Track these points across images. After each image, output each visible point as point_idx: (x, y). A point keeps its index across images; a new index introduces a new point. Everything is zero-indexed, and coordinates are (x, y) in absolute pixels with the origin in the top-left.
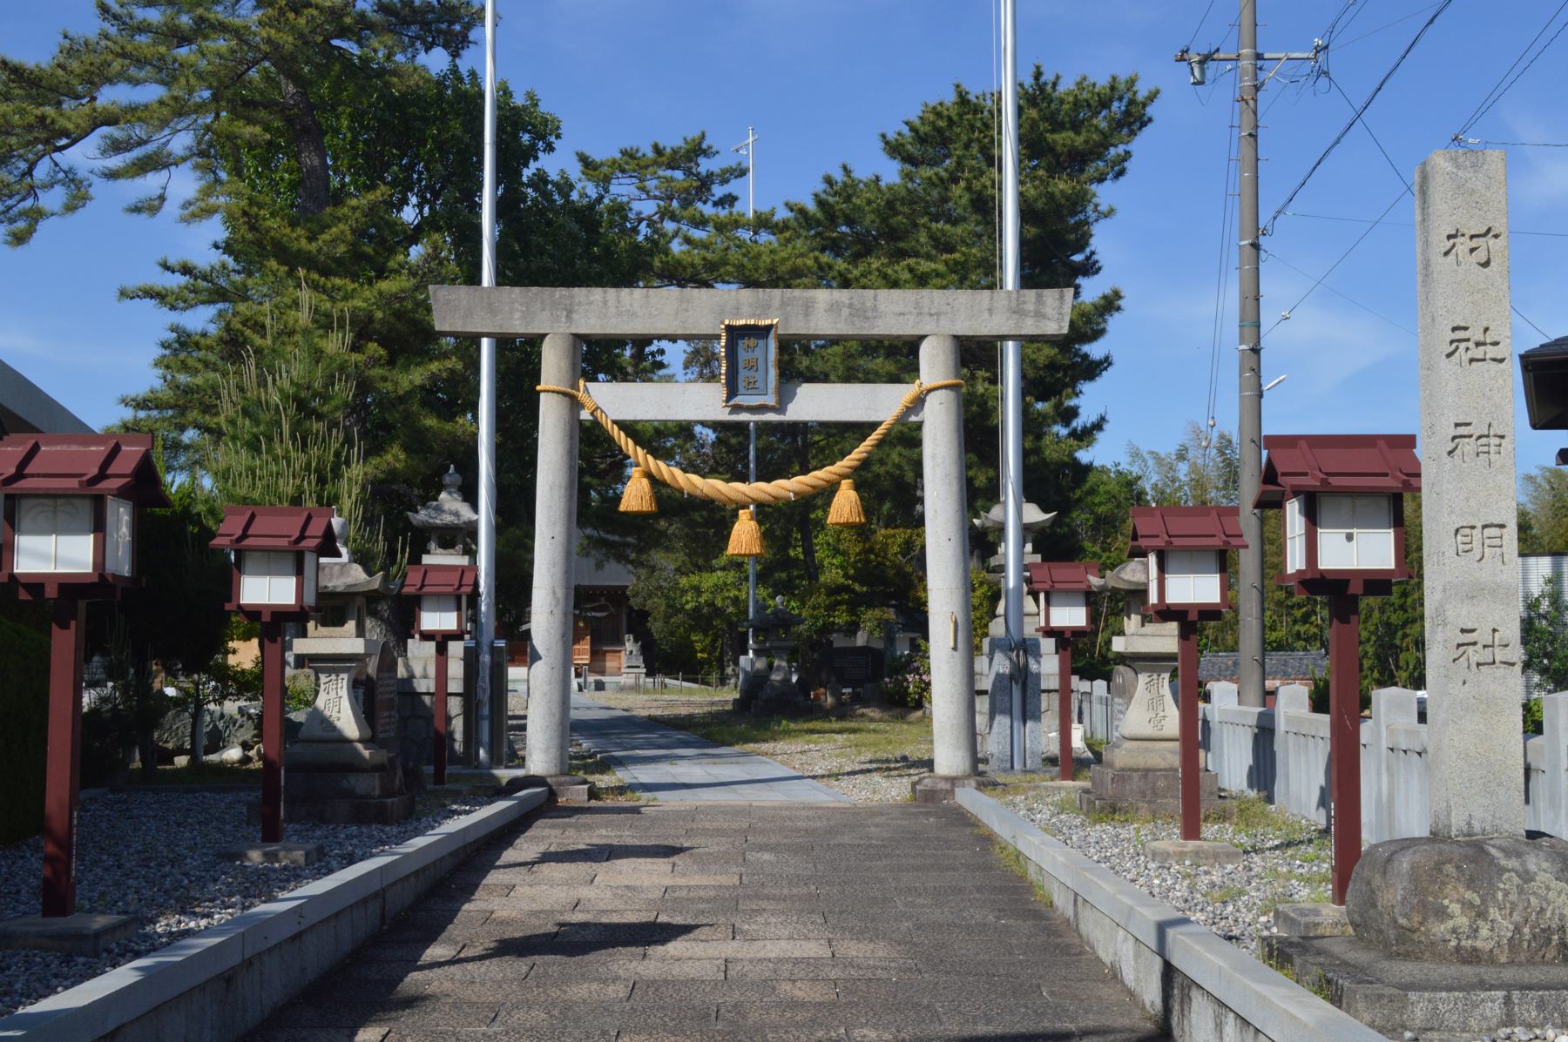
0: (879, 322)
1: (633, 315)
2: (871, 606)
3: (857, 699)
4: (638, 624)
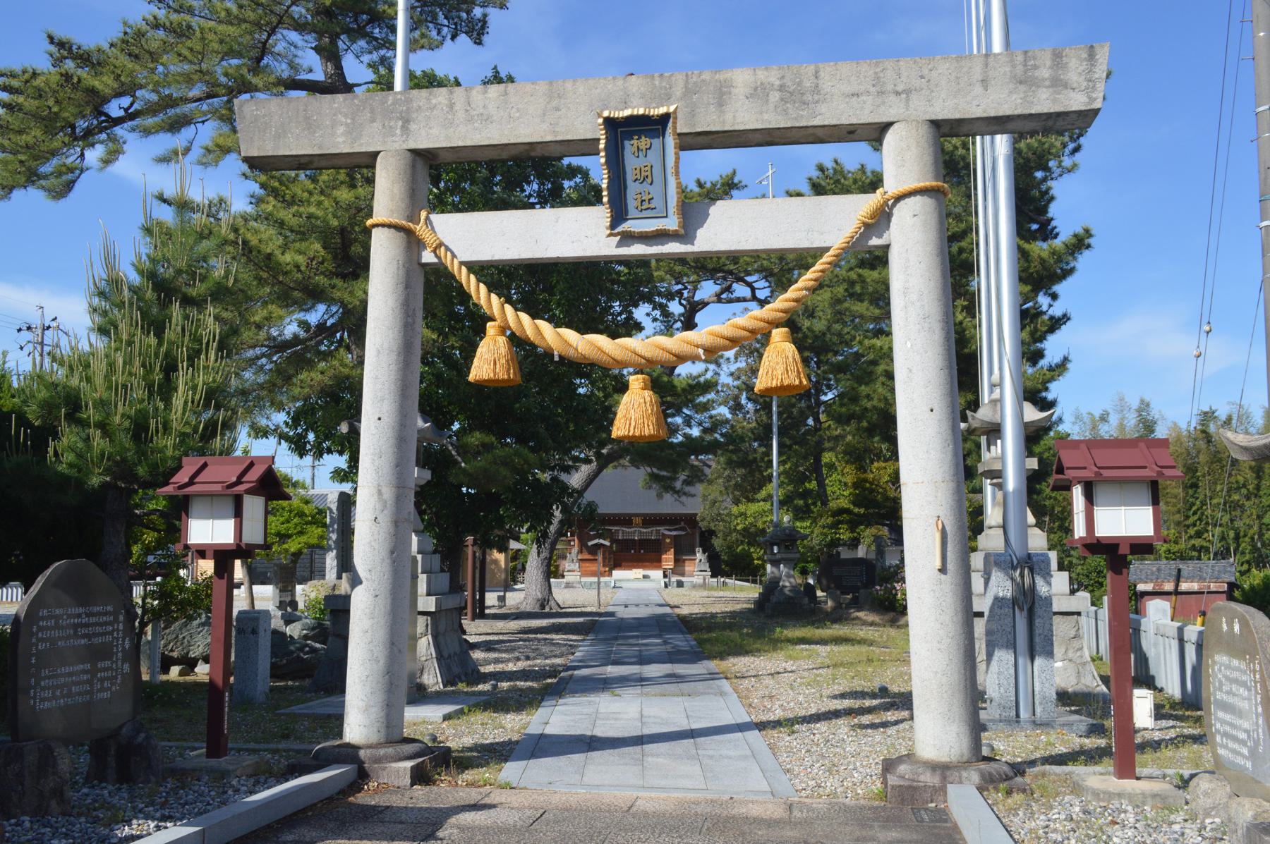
0: (823, 108)
1: (488, 119)
2: (868, 525)
3: (857, 604)
4: (706, 540)
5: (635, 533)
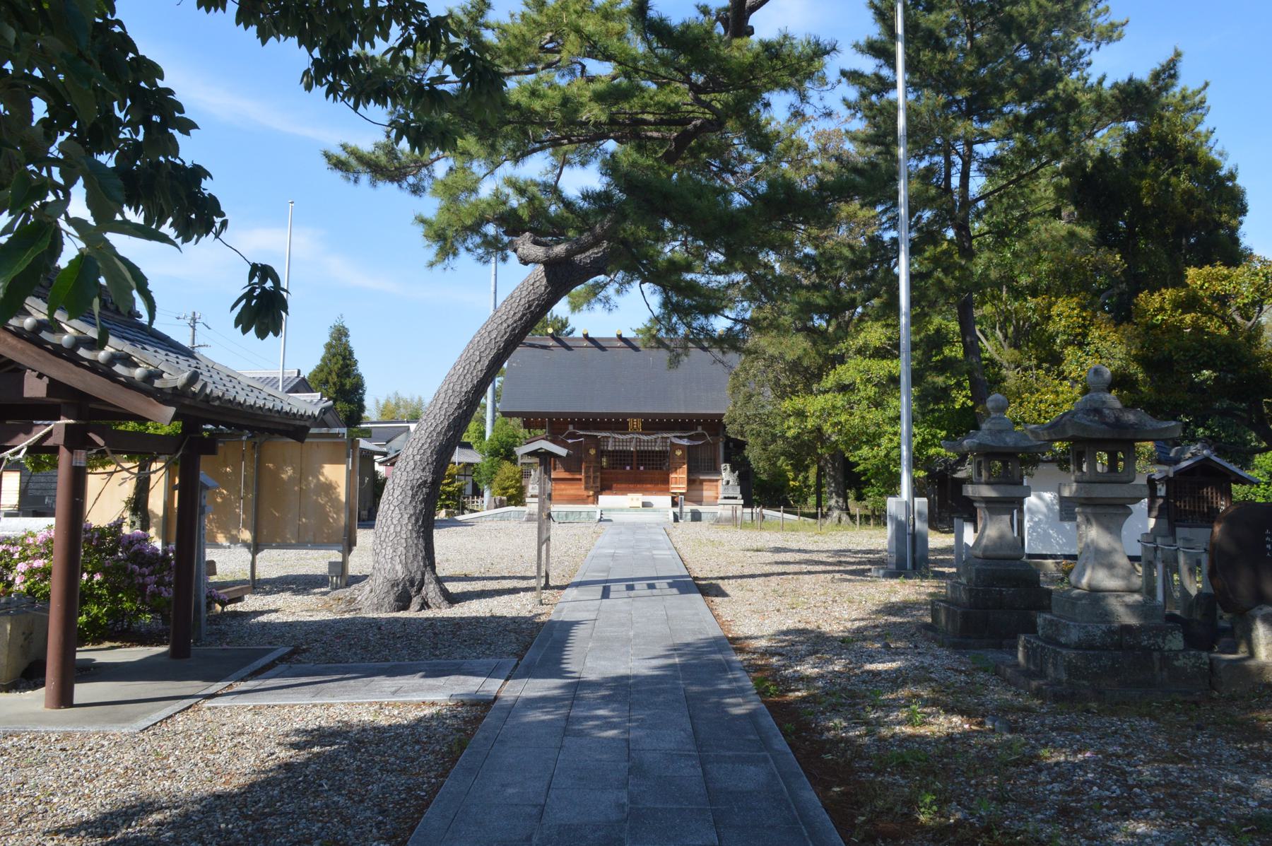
5: (630, 441)
